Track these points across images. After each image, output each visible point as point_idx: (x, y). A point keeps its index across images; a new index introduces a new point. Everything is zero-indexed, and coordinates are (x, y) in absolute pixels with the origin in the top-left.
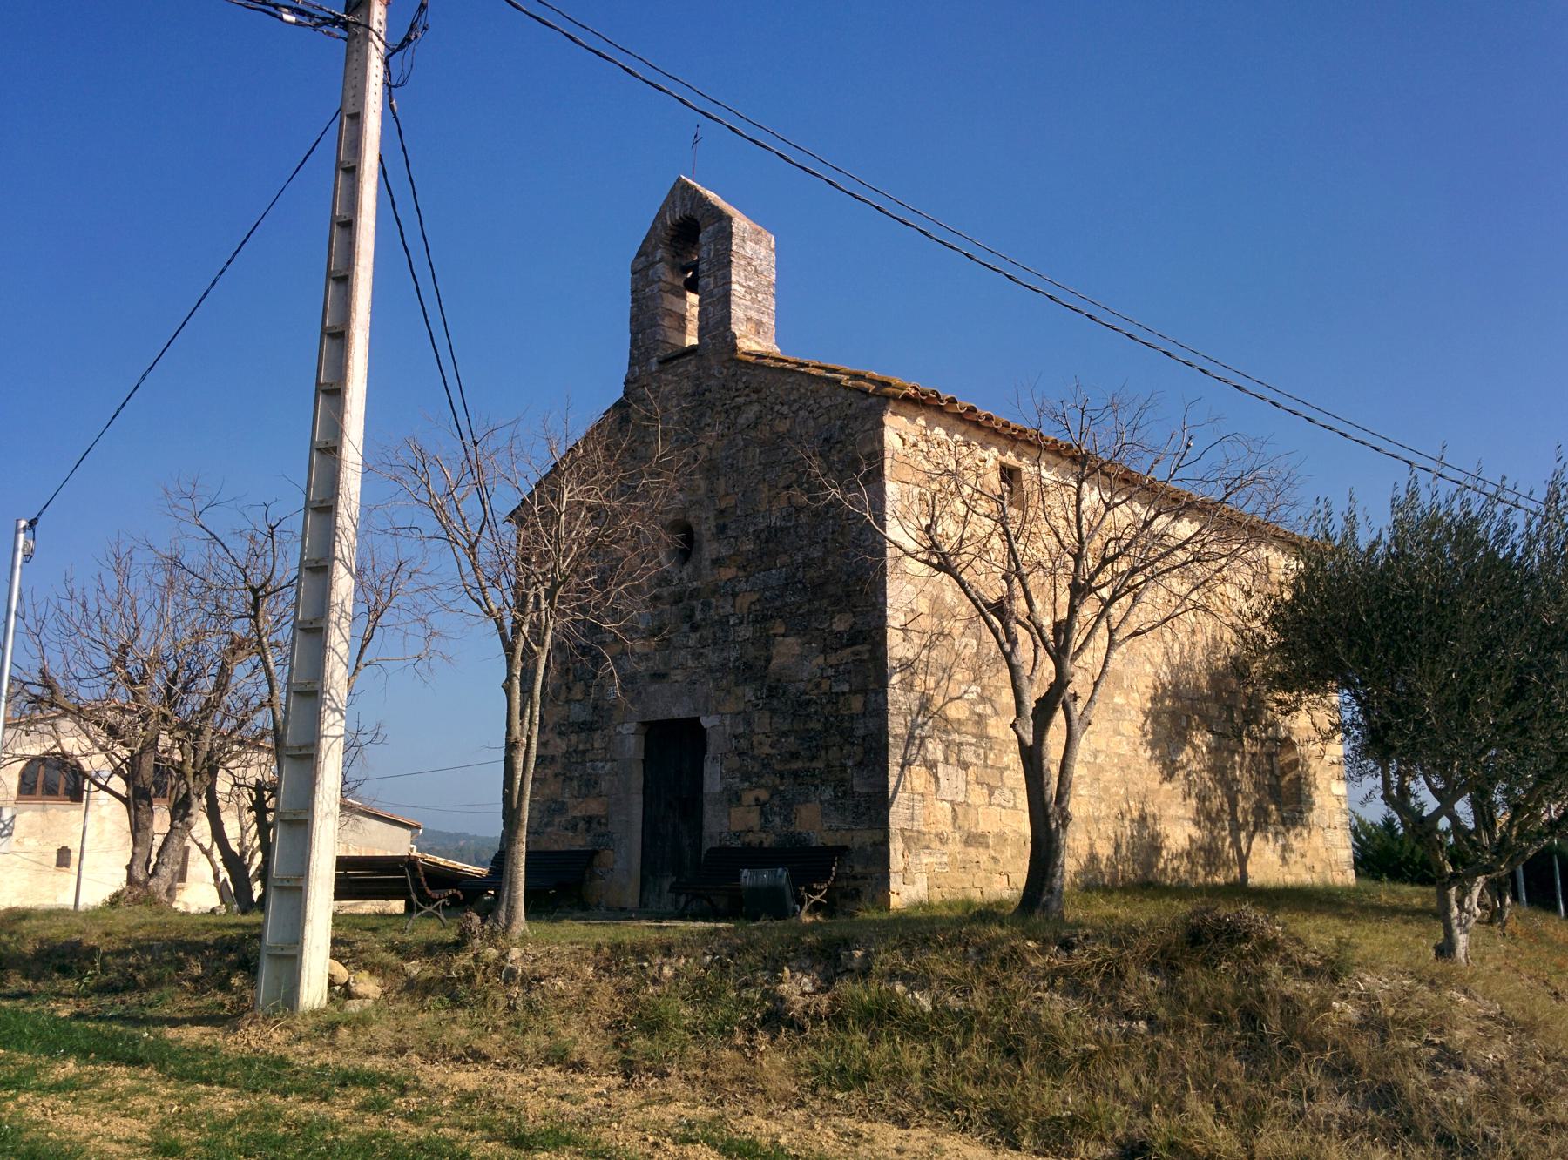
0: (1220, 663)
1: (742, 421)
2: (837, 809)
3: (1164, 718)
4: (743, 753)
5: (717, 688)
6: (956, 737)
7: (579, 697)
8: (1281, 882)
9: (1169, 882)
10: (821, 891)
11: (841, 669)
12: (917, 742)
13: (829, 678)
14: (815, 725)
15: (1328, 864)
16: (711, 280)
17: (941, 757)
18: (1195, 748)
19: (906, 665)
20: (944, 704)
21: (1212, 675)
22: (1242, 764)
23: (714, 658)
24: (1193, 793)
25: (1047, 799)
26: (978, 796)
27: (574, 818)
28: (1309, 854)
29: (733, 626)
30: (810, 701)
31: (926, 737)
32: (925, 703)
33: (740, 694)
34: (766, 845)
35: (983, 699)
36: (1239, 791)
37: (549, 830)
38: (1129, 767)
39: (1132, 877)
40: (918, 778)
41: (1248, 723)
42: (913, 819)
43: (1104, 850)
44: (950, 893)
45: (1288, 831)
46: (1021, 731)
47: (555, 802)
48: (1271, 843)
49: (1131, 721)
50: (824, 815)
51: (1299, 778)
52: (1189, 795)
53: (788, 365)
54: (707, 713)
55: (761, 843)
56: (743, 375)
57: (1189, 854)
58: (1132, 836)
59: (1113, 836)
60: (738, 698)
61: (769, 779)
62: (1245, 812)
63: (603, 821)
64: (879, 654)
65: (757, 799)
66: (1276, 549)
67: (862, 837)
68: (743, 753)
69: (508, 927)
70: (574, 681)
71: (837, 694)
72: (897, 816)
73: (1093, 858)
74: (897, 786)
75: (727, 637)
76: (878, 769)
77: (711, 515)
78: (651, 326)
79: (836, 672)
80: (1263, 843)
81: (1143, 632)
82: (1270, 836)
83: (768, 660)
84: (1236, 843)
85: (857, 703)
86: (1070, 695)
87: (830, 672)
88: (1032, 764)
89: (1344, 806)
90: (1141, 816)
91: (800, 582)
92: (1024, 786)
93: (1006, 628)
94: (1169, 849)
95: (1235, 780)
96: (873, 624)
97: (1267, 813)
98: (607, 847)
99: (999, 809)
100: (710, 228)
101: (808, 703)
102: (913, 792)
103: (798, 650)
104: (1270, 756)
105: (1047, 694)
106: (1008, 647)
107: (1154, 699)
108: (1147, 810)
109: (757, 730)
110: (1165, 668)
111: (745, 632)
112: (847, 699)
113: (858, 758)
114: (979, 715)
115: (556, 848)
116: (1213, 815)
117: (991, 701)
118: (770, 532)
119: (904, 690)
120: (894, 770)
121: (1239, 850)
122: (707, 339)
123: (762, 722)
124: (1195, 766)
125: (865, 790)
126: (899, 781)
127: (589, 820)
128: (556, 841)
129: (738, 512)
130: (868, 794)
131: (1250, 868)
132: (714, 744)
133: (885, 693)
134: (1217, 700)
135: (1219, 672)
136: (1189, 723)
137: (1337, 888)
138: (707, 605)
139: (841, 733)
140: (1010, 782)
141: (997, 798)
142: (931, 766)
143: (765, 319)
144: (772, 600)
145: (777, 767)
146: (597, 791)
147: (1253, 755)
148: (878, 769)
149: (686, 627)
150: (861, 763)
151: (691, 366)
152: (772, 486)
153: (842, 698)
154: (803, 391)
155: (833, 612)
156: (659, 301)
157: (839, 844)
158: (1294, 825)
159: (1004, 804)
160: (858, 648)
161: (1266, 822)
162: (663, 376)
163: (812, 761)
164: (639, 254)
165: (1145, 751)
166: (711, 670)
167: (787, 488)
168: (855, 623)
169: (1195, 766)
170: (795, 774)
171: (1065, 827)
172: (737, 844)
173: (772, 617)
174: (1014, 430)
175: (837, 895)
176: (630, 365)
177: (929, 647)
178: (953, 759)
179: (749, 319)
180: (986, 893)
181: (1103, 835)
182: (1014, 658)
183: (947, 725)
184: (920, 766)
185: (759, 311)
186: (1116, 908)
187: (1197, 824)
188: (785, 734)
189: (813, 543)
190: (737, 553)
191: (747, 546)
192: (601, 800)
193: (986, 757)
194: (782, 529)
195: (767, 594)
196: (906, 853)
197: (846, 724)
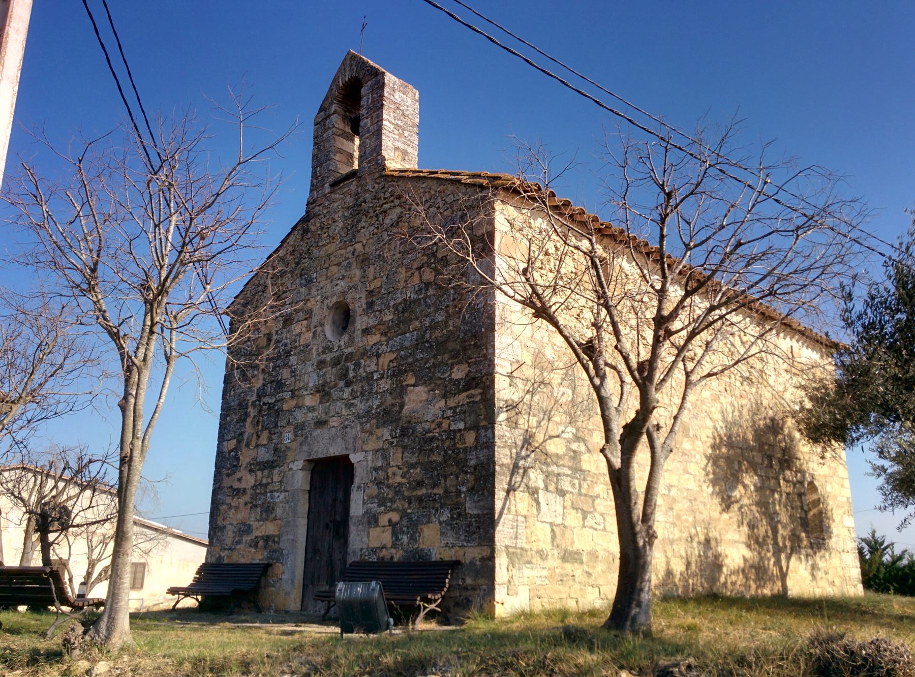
0: (762, 423)
1: (388, 221)
2: (452, 528)
3: (722, 462)
4: (381, 483)
5: (363, 431)
6: (554, 469)
7: (265, 442)
8: (812, 595)
9: (729, 593)
10: (435, 601)
11: (458, 410)
12: (521, 471)
13: (448, 418)
14: (437, 458)
15: (844, 579)
16: (369, 120)
17: (541, 485)
18: (745, 487)
19: (512, 407)
20: (545, 441)
21: (756, 431)
22: (780, 501)
23: (361, 406)
24: (745, 522)
25: (635, 518)
26: (573, 519)
27: (257, 537)
28: (830, 571)
29: (376, 380)
30: (433, 437)
31: (529, 468)
32: (528, 440)
33: (380, 435)
34: (396, 560)
35: (577, 438)
36: (779, 521)
37: (238, 547)
38: (695, 500)
39: (700, 589)
40: (521, 501)
41: (782, 469)
42: (516, 538)
43: (678, 567)
44: (549, 603)
45: (815, 553)
46: (609, 455)
47: (245, 524)
48: (804, 563)
49: (697, 463)
50: (442, 534)
51: (821, 513)
52: (742, 523)
53: (422, 174)
54: (355, 450)
55: (392, 557)
56: (389, 187)
57: (743, 571)
58: (700, 556)
59: (684, 555)
60: (378, 438)
61: (398, 504)
62: (784, 538)
63: (276, 539)
64: (488, 396)
65: (390, 521)
66: (798, 341)
67: (472, 553)
68: (381, 483)
69: (108, 637)
70: (262, 431)
71: (454, 431)
72: (503, 535)
73: (669, 573)
74: (503, 508)
75: (372, 389)
76: (486, 493)
77: (363, 296)
78: (326, 161)
79: (455, 412)
80: (798, 563)
81: (716, 374)
82: (802, 557)
83: (402, 406)
84: (778, 562)
85: (470, 438)
86: (654, 426)
87: (450, 413)
88: (620, 485)
89: (853, 535)
90: (706, 539)
91: (428, 342)
92: (614, 511)
93: (596, 367)
94: (728, 567)
95: (776, 513)
96: (484, 371)
97: (799, 539)
98: (278, 560)
99: (591, 531)
100: (369, 83)
101: (432, 439)
102: (517, 514)
103: (424, 396)
104: (800, 495)
105: (633, 420)
106: (597, 381)
107: (713, 447)
108: (710, 535)
109: (392, 463)
110: (721, 423)
111: (385, 385)
112: (462, 435)
113: (470, 485)
114: (575, 452)
115: (243, 561)
116: (761, 540)
117: (584, 441)
118: (405, 304)
119: (509, 426)
120: (500, 495)
121: (781, 568)
122: (365, 164)
123: (396, 457)
124: (746, 501)
125: (475, 512)
126: (504, 504)
127: (267, 539)
128: (243, 556)
129: (383, 291)
130: (478, 516)
131: (789, 583)
132: (360, 476)
133: (493, 428)
134: (760, 451)
135: (761, 430)
136: (740, 467)
137: (851, 599)
138: (357, 365)
139: (457, 464)
140: (600, 508)
141: (590, 521)
142: (533, 492)
143: (410, 150)
144: (406, 357)
145: (406, 493)
146: (273, 515)
147: (788, 494)
148: (486, 493)
149: (341, 384)
150: (472, 489)
151: (353, 185)
152: (408, 268)
153: (458, 435)
154: (433, 192)
155: (452, 364)
156: (333, 141)
157: (454, 559)
158: (819, 548)
159: (596, 526)
160: (472, 392)
161: (799, 547)
162: (333, 196)
163: (433, 488)
164: (320, 111)
165: (708, 487)
166: (359, 417)
167: (419, 268)
168: (469, 372)
169: (746, 501)
170: (420, 500)
171: (651, 544)
172: (374, 559)
173: (405, 371)
174: (602, 225)
175: (451, 604)
176: (311, 191)
177: (532, 392)
178: (552, 487)
179: (397, 149)
180: (581, 601)
181: (677, 554)
182: (603, 391)
183: (547, 458)
184: (523, 491)
185: (404, 143)
186: (693, 618)
187: (749, 546)
188: (413, 466)
189: (437, 310)
190: (381, 323)
191: (388, 317)
192: (276, 522)
193: (580, 487)
194: (414, 301)
195: (402, 353)
196: (510, 567)
197: (461, 456)
